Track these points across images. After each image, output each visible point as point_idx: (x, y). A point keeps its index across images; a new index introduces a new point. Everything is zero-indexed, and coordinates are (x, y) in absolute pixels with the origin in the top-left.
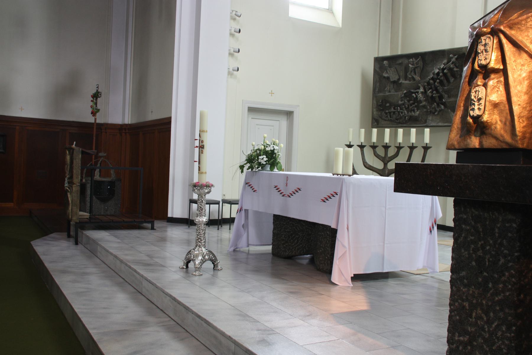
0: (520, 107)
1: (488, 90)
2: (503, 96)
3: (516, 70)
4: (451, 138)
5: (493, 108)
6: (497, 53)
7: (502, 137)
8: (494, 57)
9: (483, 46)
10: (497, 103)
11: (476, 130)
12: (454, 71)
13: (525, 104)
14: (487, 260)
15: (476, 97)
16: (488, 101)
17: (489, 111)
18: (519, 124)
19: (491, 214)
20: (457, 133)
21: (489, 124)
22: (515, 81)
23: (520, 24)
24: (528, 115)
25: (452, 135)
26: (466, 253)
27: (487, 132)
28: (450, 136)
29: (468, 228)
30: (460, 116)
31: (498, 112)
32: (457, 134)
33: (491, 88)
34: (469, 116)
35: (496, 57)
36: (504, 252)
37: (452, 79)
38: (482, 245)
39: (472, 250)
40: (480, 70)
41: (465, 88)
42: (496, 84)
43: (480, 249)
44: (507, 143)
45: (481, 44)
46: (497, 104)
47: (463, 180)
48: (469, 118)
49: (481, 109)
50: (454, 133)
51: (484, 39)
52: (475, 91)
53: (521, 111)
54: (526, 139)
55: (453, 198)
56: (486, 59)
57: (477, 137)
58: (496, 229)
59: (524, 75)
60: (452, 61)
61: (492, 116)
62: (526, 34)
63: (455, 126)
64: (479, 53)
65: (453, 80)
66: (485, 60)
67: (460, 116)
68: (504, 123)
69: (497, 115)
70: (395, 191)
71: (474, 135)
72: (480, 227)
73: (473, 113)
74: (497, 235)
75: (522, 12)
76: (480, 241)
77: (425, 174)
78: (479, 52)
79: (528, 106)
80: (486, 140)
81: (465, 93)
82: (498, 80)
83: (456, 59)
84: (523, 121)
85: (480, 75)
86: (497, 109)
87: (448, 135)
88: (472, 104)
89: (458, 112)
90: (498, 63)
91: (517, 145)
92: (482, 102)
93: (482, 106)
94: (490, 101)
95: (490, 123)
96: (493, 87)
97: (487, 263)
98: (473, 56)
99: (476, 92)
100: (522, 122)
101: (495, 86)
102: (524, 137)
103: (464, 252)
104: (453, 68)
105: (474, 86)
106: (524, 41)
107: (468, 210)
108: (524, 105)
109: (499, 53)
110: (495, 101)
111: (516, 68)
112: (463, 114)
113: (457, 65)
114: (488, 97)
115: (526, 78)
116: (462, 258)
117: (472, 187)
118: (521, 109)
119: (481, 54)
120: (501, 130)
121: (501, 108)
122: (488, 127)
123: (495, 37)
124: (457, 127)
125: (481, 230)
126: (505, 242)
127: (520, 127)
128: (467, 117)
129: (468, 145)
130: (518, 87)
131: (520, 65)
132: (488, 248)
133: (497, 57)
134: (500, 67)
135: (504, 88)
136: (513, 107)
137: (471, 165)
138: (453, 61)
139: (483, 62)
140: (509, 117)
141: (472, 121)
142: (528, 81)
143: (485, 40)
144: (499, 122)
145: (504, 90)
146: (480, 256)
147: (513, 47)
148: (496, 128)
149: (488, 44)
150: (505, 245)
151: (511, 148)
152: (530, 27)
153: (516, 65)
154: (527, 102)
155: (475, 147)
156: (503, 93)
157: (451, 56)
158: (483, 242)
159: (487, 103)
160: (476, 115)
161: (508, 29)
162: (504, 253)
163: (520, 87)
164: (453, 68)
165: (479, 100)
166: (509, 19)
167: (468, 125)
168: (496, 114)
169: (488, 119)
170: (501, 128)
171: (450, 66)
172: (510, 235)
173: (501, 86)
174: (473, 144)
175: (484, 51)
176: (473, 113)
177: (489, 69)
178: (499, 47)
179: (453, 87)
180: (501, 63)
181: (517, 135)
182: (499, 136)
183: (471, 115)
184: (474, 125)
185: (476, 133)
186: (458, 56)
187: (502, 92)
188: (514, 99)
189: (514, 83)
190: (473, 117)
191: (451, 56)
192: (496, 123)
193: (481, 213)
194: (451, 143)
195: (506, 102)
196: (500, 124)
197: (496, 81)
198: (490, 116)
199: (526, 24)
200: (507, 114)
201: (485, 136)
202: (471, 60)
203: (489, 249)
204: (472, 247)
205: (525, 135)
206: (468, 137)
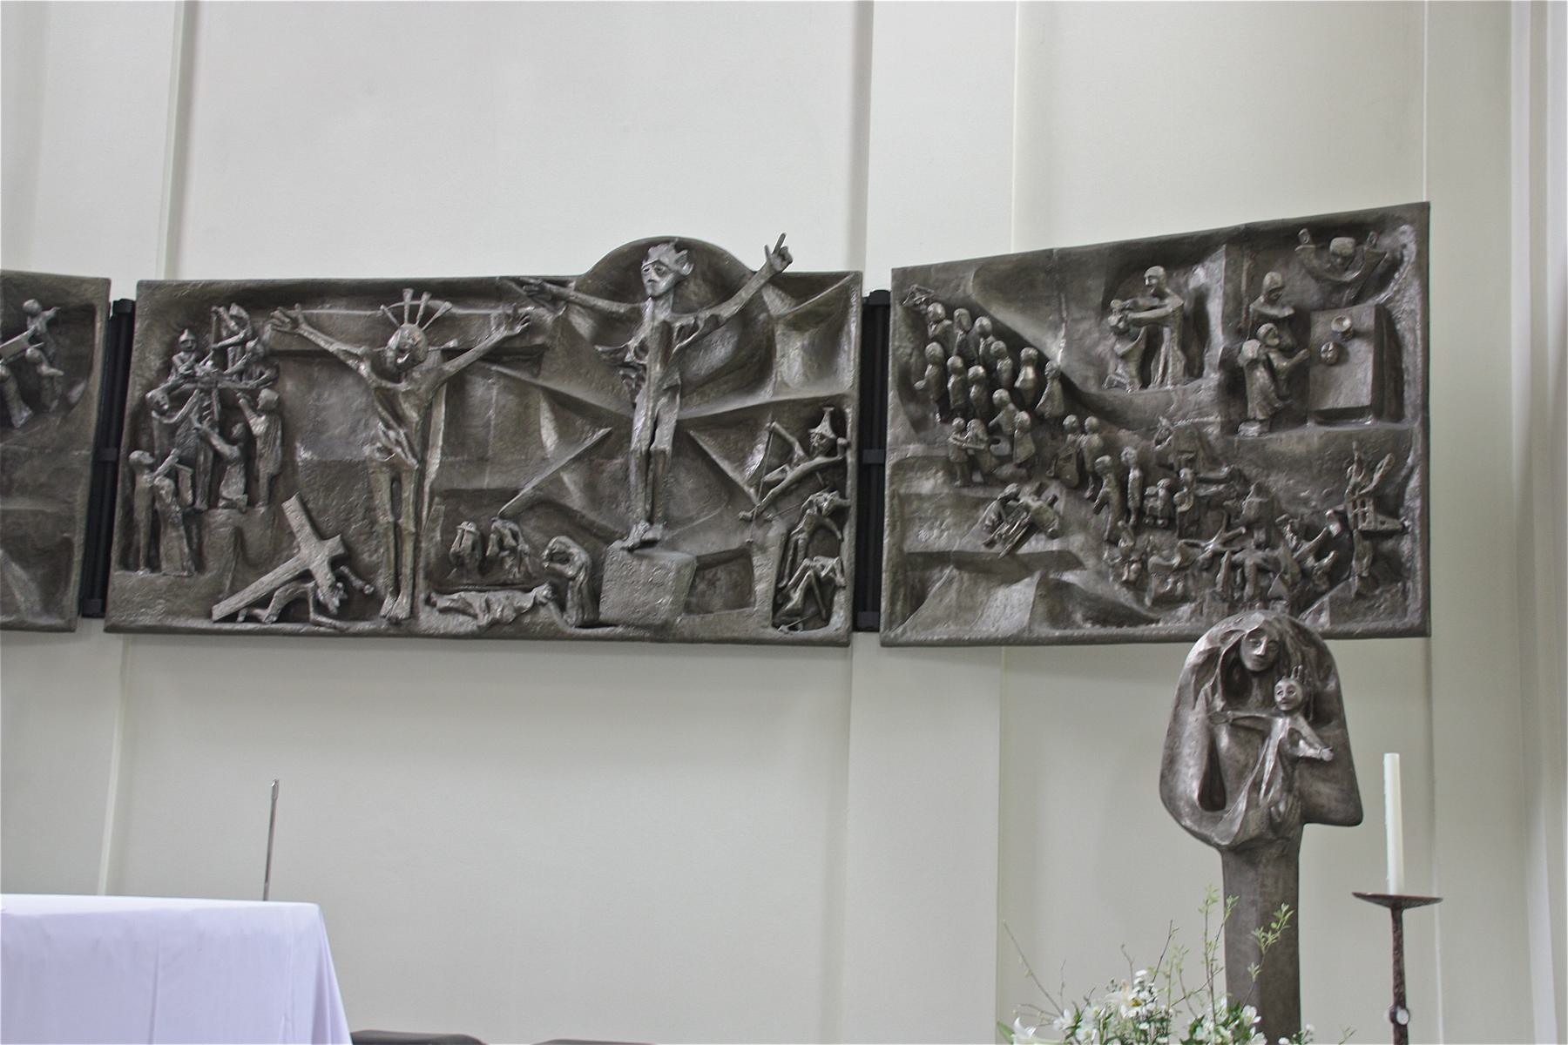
12: (40, 377)
37: (20, 410)
60: (32, 328)
65: (25, 414)
70: (893, 270)
83: (51, 323)
104: (36, 363)
113: (50, 353)
137: (892, 484)
138: (36, 330)
157: (30, 304)
164: (36, 363)
171: (25, 350)
179: (24, 449)
186: (57, 313)
191: (30, 304)
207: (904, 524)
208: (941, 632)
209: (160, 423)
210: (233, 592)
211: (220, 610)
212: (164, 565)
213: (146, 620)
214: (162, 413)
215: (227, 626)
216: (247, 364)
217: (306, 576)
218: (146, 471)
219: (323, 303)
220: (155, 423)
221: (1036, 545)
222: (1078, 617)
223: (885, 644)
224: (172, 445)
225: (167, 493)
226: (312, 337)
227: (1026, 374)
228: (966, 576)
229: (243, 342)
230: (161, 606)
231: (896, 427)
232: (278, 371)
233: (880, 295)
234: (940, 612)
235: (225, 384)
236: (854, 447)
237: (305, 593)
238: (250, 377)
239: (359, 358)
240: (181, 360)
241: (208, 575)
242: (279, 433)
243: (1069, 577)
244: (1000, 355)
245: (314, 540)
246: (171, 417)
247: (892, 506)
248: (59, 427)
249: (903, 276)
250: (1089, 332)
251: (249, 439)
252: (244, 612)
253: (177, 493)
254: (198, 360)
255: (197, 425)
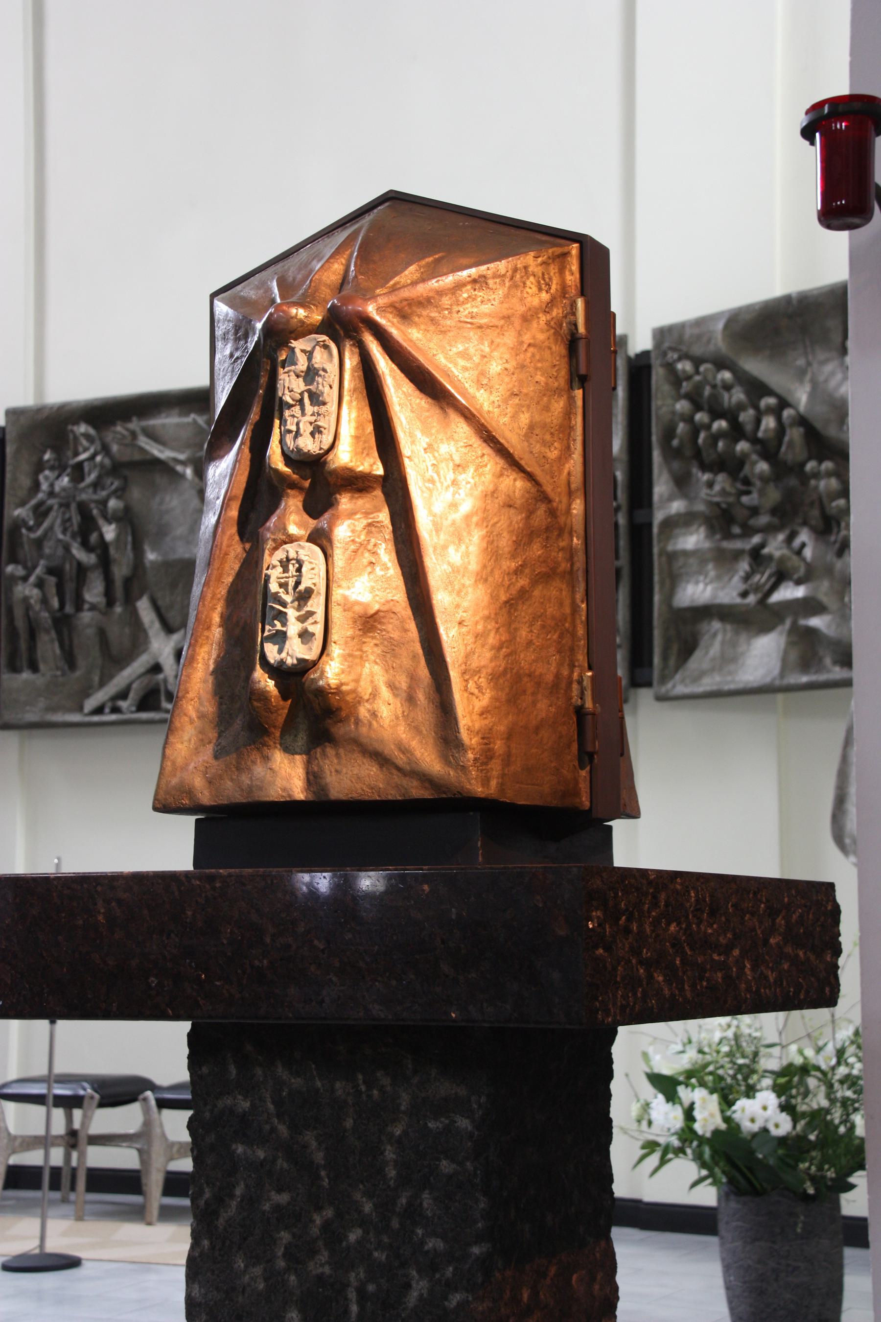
0: (464, 630)
1: (336, 558)
2: (394, 585)
3: (438, 484)
4: (174, 763)
5: (358, 632)
6: (359, 409)
7: (403, 753)
8: (347, 431)
9: (301, 379)
10: (372, 612)
11: (289, 726)
13: (482, 622)
14: (352, 1295)
15: (290, 588)
16: (339, 605)
17: (346, 643)
18: (468, 699)
19: (361, 1082)
20: (202, 740)
21: (349, 698)
22: (437, 528)
23: (436, 307)
24: (493, 664)
25: (179, 746)
26: (258, 1271)
27: (340, 730)
28: (168, 752)
29: (261, 1154)
30: (208, 665)
31: (378, 651)
32: (202, 742)
33: (349, 552)
34: (258, 667)
35: (357, 428)
36: (426, 1248)
38: (326, 1225)
39: (284, 1255)
40: (295, 476)
41: (229, 546)
42: (363, 537)
43: (320, 1243)
44: (425, 779)
45: (293, 368)
46: (372, 616)
47: (268, 940)
48: (259, 674)
49: (313, 634)
50: (186, 738)
51: (303, 351)
52: (281, 561)
53: (469, 648)
54: (494, 761)
55: (186, 1026)
56: (317, 431)
57: (294, 753)
58: (389, 1147)
59: (467, 506)
61: (356, 664)
62: (460, 347)
63: (190, 708)
64: (287, 403)
66: (312, 434)
67: (212, 667)
68: (404, 695)
69: (376, 663)
71: (281, 744)
72: (314, 1144)
73: (280, 651)
74: (392, 1173)
75: (432, 262)
76: (319, 1208)
77: (81, 922)
78: (287, 399)
79: (490, 630)
80: (338, 767)
81: (227, 568)
82: (370, 521)
84: (479, 688)
85: (294, 497)
86: (373, 638)
87: (161, 746)
88: (269, 614)
89: (201, 646)
90: (365, 452)
91: (468, 787)
92: (316, 605)
93: (316, 622)
94: (348, 606)
95: (354, 695)
96: (353, 547)
97: (354, 1308)
98: (254, 415)
99: (285, 564)
100: (476, 691)
101: (361, 544)
102: (486, 755)
103: (246, 1267)
105: (274, 540)
106: (457, 373)
107: (259, 1071)
108: (477, 623)
109: (367, 414)
110: (366, 606)
111: (439, 475)
112: (223, 658)
114: (339, 586)
115: (475, 519)
116: (240, 1299)
117: (313, 968)
118: (470, 639)
119: (297, 410)
120: (397, 725)
121: (388, 632)
122: (343, 714)
123: (348, 346)
124: (198, 711)
125: (319, 1157)
126: (427, 1200)
127: (471, 713)
128: (252, 669)
129: (261, 788)
130: (451, 549)
131: (451, 465)
132: (353, 1236)
133: (360, 426)
134: (375, 467)
135: (394, 555)
136: (442, 630)
137: (659, 541)
139: (308, 444)
140: (423, 672)
141: (275, 685)
142: (484, 532)
143: (310, 355)
144: (385, 693)
145: (396, 561)
146: (320, 1278)
147: (417, 393)
148: (374, 714)
149: (321, 373)
150: (429, 1213)
151: (444, 796)
152: (471, 323)
153: (435, 462)
154: (486, 612)
155: (290, 796)
156: (391, 572)
158: (329, 1213)
159: (336, 614)
160: (295, 662)
161: (395, 320)
162: (428, 1252)
163: (459, 554)
165: (304, 597)
166: (391, 283)
167: (256, 704)
168: (372, 658)
169: (344, 678)
170: (397, 718)
172: (446, 1166)
173: (384, 546)
174: (279, 783)
175: (307, 401)
176: (280, 651)
177: (334, 472)
178: (361, 386)
180: (376, 454)
181: (463, 745)
182: (391, 750)
183: (272, 661)
184: (282, 703)
185: (289, 739)
187: (388, 569)
188: (441, 599)
189: (434, 533)
190: (277, 671)
192: (375, 695)
193: (319, 1084)
194: (174, 781)
195: (409, 612)
196: (391, 702)
197: (365, 522)
198: (349, 667)
199: (455, 308)
200: (415, 657)
201: (330, 751)
202: (244, 434)
203: (359, 1242)
204: (284, 1241)
205: (492, 746)
206: (255, 755)
207: (673, 581)
208: (707, 684)
209: (28, 537)
210: (102, 684)
211: (90, 704)
212: (42, 667)
213: (31, 717)
214: (30, 529)
215: (96, 718)
216: (99, 478)
217: (156, 668)
218: (20, 582)
219: (159, 413)
220: (25, 539)
221: (790, 592)
222: (828, 661)
223: (660, 698)
224: (41, 556)
225: (36, 602)
226: (147, 447)
227: (767, 424)
228: (729, 627)
229: (92, 458)
230: (42, 703)
231: (661, 487)
232: (125, 479)
233: (645, 354)
234: (705, 665)
235: (84, 497)
236: (624, 508)
237: (158, 684)
238: (103, 489)
239: (183, 463)
240: (45, 478)
241: (78, 673)
242: (130, 539)
243: (815, 622)
244: (741, 407)
245: (162, 634)
246: (35, 532)
247: (660, 564)
248: (272, 533)
249: (661, 334)
250: (832, 374)
251: (104, 545)
252: (109, 705)
253: (45, 601)
254: (58, 478)
255: (61, 536)
